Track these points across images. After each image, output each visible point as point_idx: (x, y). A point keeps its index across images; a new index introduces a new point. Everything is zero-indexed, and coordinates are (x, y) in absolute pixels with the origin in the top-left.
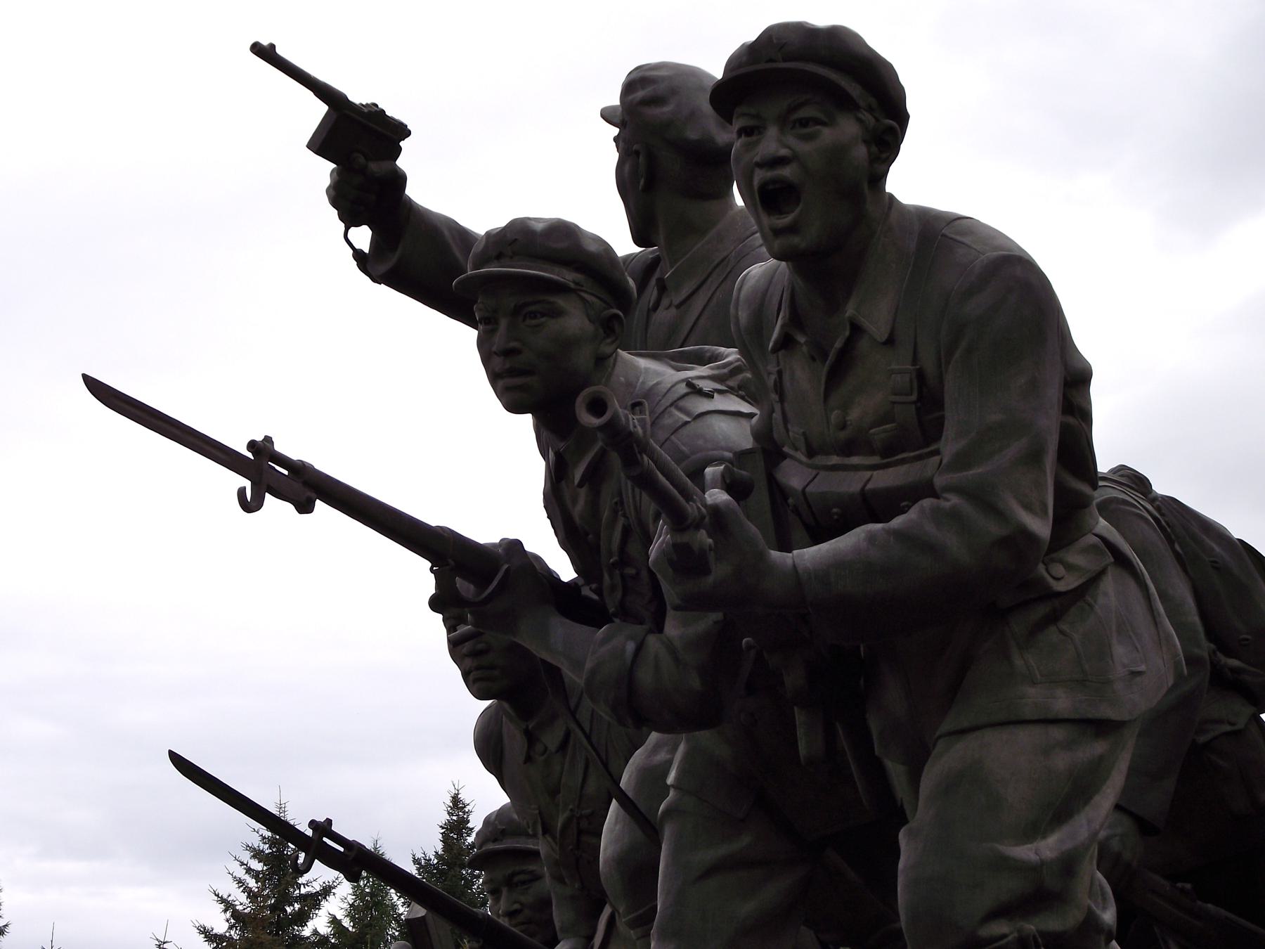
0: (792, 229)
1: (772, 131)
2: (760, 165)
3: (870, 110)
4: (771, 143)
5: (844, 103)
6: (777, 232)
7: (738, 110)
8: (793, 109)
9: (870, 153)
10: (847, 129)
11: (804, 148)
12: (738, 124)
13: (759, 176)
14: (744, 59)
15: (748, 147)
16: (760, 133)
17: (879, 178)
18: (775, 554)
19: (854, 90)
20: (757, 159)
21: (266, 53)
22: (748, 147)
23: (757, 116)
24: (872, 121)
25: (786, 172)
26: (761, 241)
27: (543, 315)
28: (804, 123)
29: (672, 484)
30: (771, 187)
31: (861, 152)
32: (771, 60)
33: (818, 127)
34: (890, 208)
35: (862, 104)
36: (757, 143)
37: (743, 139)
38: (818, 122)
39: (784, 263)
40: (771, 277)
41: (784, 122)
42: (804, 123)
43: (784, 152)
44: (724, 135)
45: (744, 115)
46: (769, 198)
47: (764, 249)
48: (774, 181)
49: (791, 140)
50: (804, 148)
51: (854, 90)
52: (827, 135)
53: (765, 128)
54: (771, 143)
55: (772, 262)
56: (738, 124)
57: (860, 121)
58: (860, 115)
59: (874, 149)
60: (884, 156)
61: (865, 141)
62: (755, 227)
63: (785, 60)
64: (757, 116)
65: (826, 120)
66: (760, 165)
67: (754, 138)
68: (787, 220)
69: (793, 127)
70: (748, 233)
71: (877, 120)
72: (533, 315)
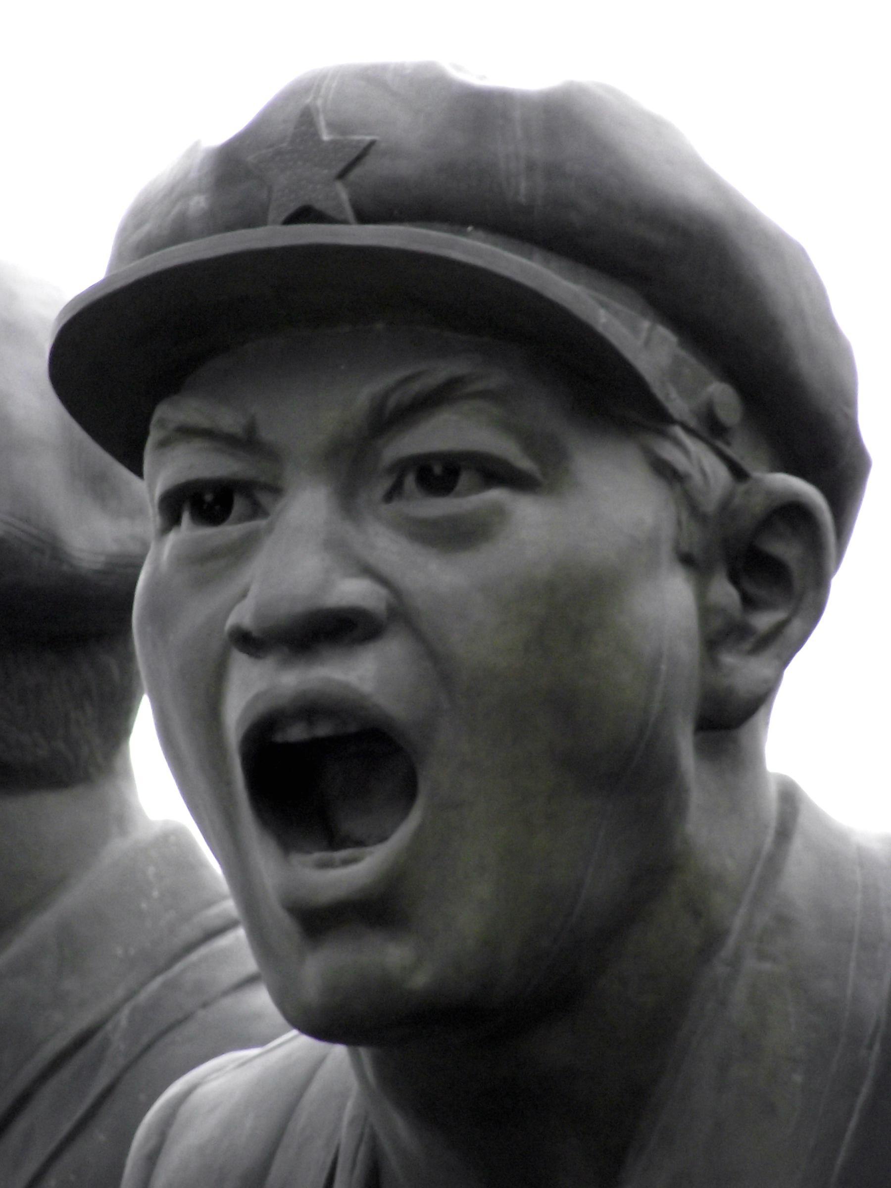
0: (376, 910)
1: (307, 506)
2: (248, 642)
3: (712, 430)
4: (303, 551)
5: (606, 397)
6: (318, 921)
7: (168, 414)
8: (388, 419)
9: (705, 611)
10: (613, 508)
11: (434, 576)
12: (169, 467)
13: (251, 687)
14: (199, 203)
15: (207, 567)
16: (257, 511)
17: (729, 720)
18: (152, 786)
19: (648, 346)
20: (243, 616)
22: (207, 567)
23: (246, 442)
24: (720, 474)
25: (361, 674)
26: (250, 964)
28: (439, 474)
29: (229, 783)
30: (296, 733)
31: (670, 605)
32: (305, 214)
33: (496, 495)
34: (785, 832)
35: (677, 404)
36: (239, 552)
37: (187, 530)
38: (495, 473)
39: (339, 1052)
40: (285, 1106)
41: (352, 465)
42: (439, 474)
43: (353, 591)
44: (108, 520)
45: (187, 432)
46: (295, 778)
47: (261, 999)
48: (309, 708)
49: (386, 546)
50: (434, 576)
51: (648, 346)
52: (533, 529)
53: (276, 491)
54: (303, 551)
55: (294, 1045)
56: (169, 467)
57: (666, 472)
58: (669, 453)
59: (724, 592)
60: (763, 621)
61: (687, 560)
62: (229, 906)
63: (363, 217)
64: (246, 442)
65: (524, 463)
66: (248, 642)
67: (230, 531)
68: (353, 872)
69: (394, 493)
70: (188, 932)
71: (738, 473)
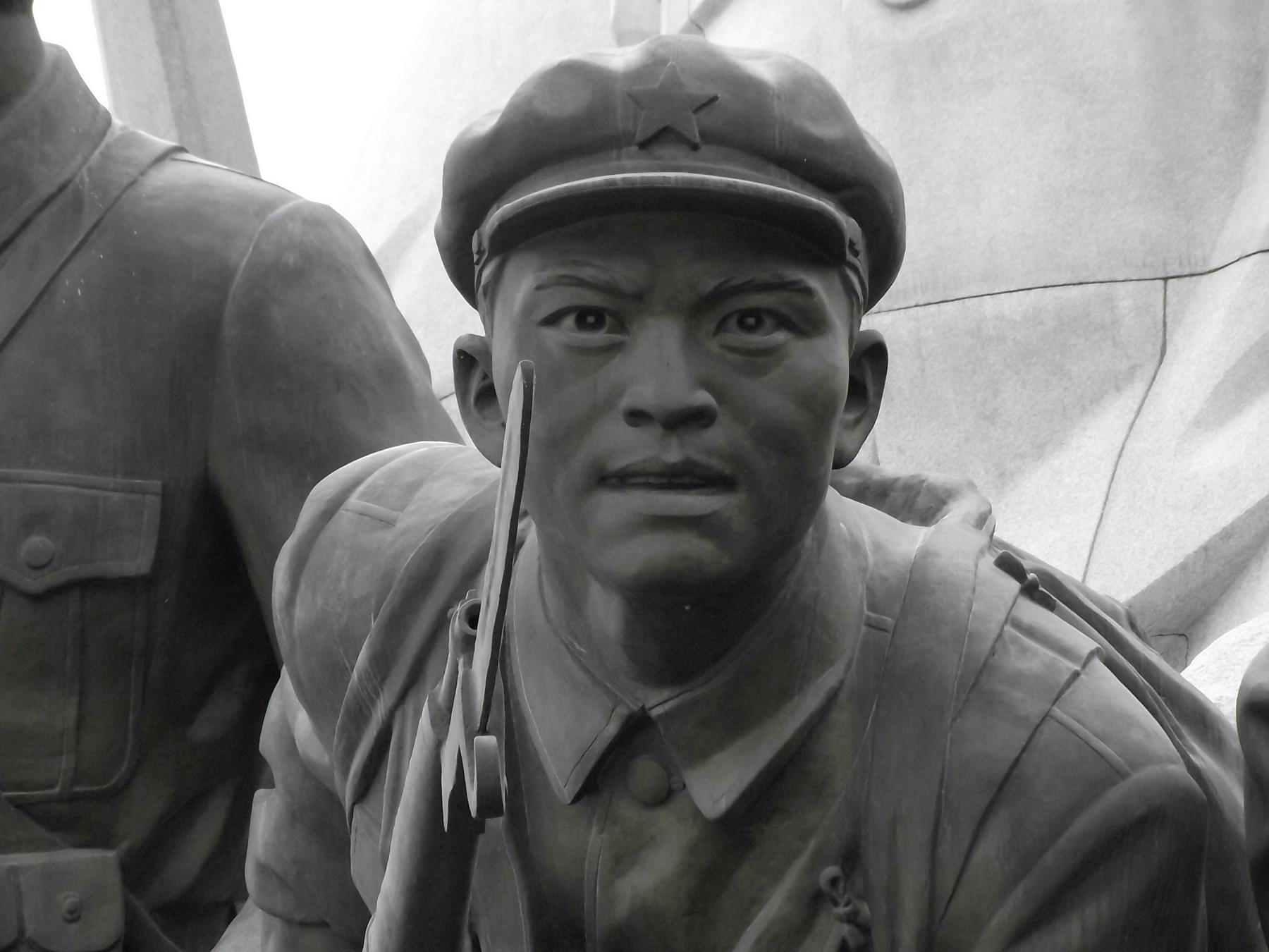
27: (783, 322)
72: (751, 320)
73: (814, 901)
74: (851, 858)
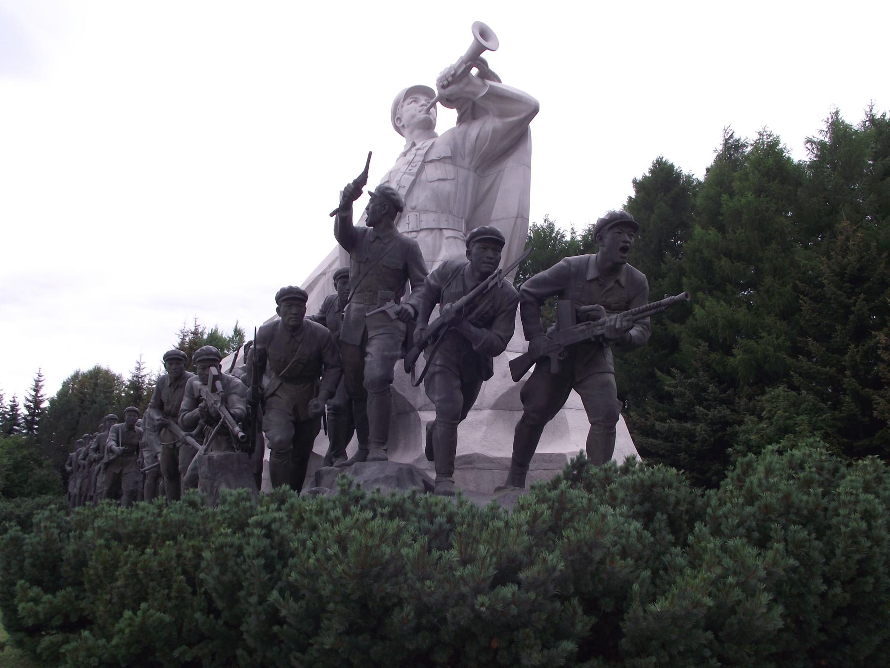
21: (370, 154)
73: (490, 301)
74: (494, 298)
